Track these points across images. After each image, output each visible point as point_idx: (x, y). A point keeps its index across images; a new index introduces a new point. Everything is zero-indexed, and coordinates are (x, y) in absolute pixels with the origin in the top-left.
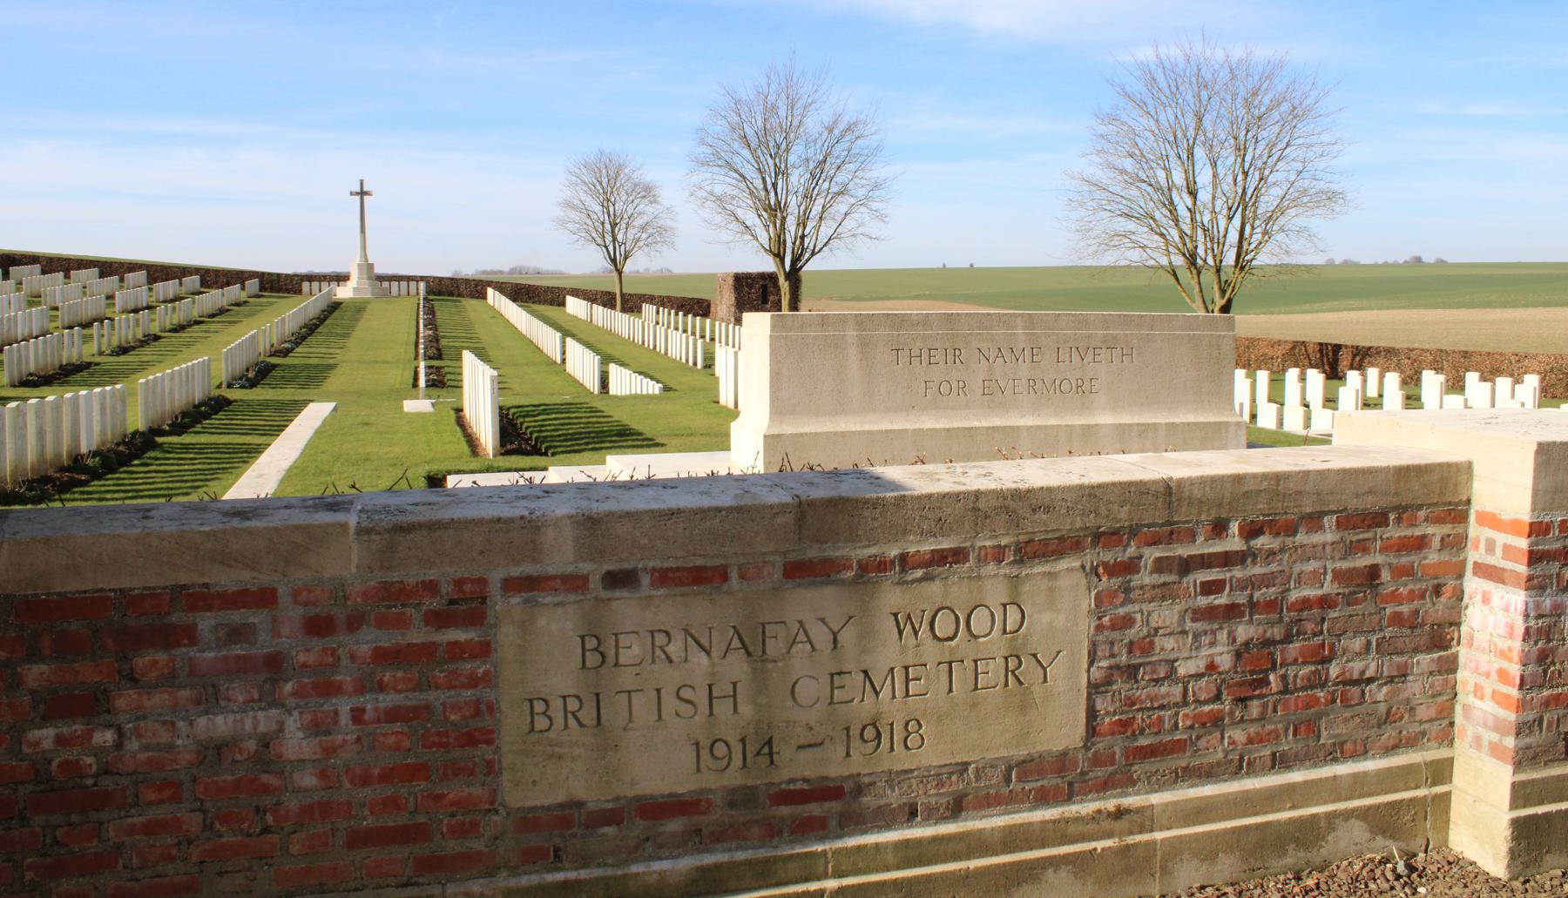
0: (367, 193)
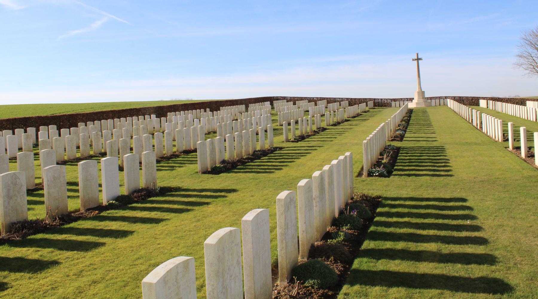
0: (420, 59)
